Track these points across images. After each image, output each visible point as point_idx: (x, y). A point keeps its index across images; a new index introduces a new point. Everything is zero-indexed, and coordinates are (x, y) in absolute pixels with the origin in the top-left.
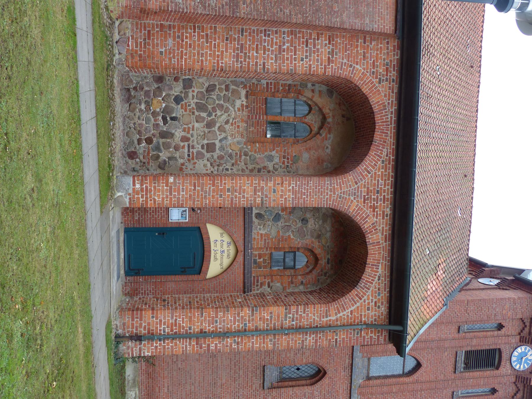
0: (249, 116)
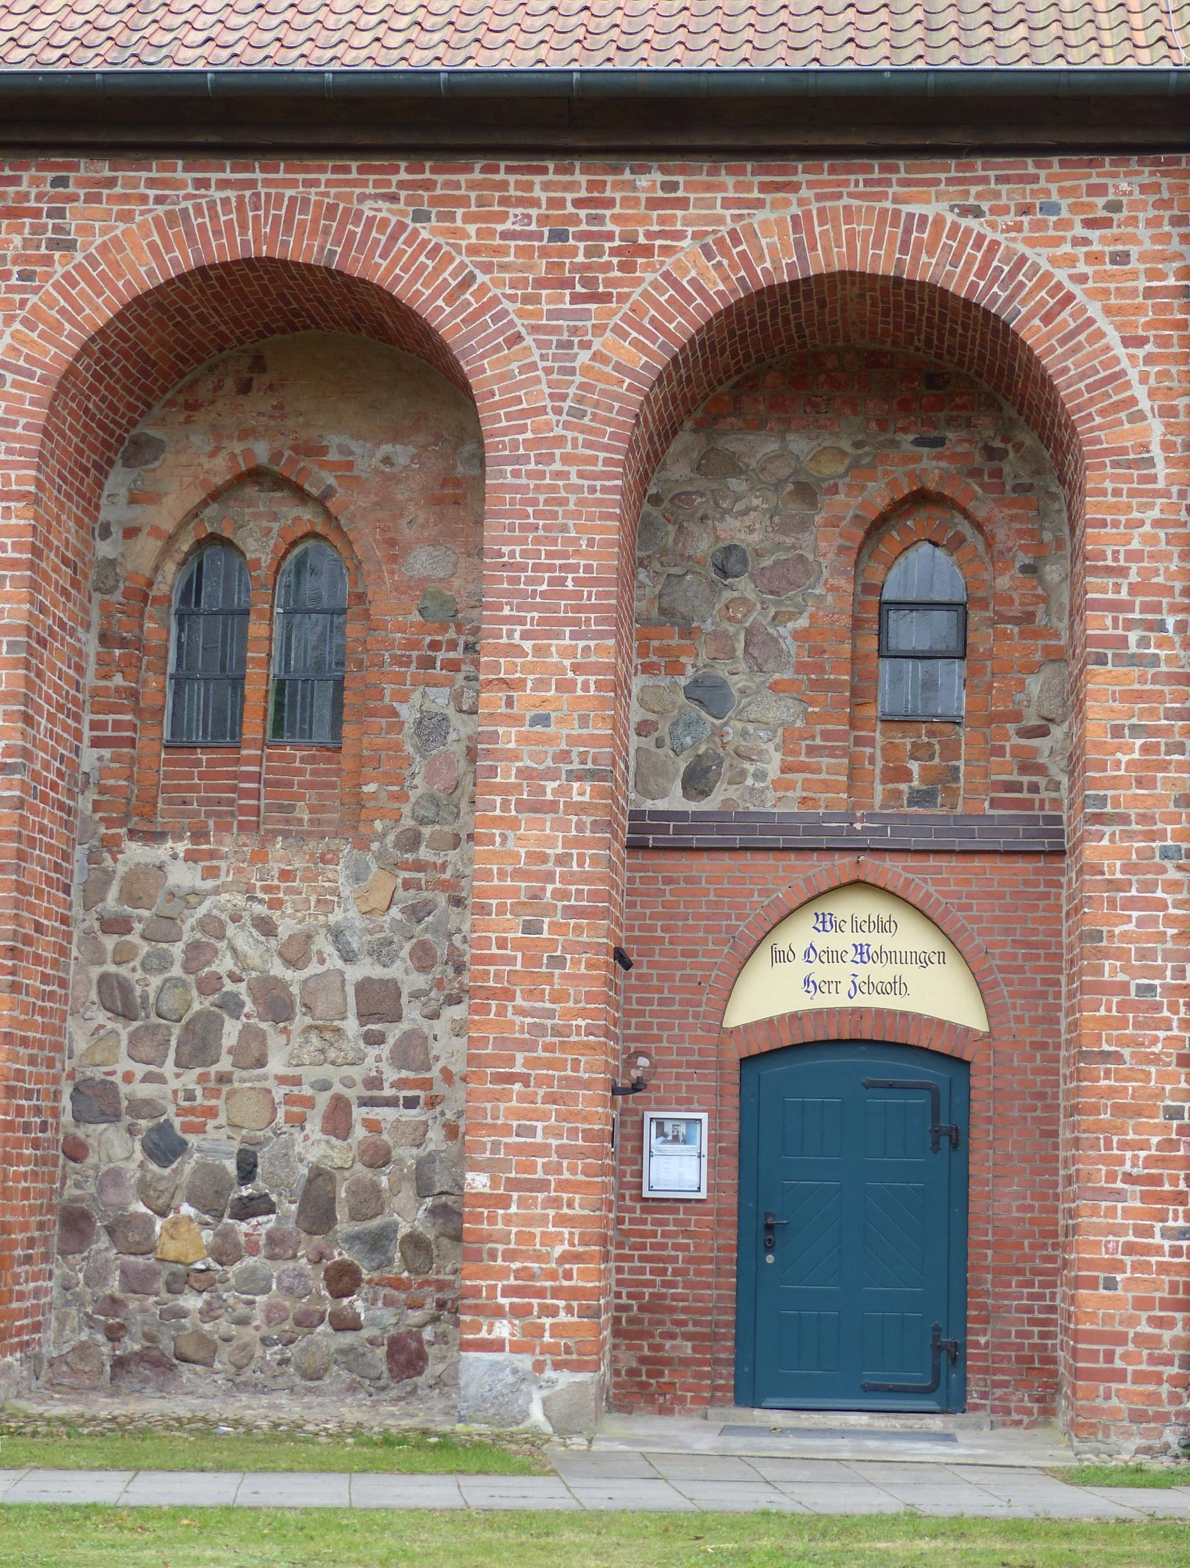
0: (242, 826)
